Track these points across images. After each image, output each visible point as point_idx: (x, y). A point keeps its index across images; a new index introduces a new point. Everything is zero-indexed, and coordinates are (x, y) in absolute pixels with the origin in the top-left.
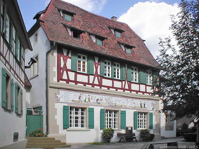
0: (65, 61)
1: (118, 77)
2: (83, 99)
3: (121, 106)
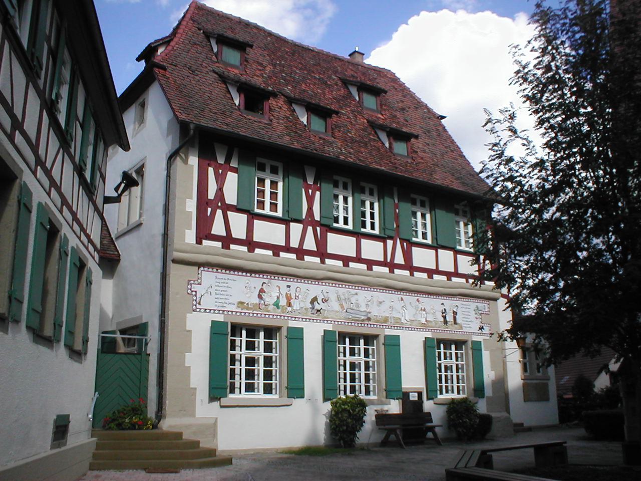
0: (221, 180)
1: (373, 228)
2: (270, 298)
3: (386, 320)
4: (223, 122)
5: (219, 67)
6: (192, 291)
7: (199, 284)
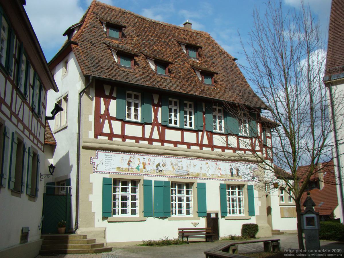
0: (107, 105)
2: (134, 165)
3: (198, 175)
6: (93, 163)
7: (96, 159)
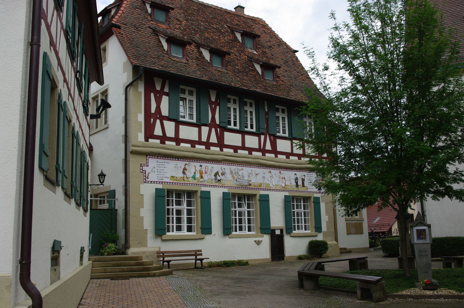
1: (252, 127)
2: (190, 174)
3: (260, 185)
4: (159, 64)
5: (153, 24)
